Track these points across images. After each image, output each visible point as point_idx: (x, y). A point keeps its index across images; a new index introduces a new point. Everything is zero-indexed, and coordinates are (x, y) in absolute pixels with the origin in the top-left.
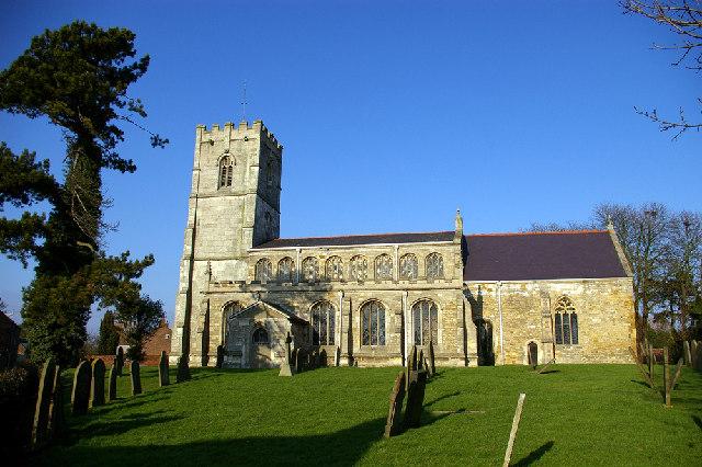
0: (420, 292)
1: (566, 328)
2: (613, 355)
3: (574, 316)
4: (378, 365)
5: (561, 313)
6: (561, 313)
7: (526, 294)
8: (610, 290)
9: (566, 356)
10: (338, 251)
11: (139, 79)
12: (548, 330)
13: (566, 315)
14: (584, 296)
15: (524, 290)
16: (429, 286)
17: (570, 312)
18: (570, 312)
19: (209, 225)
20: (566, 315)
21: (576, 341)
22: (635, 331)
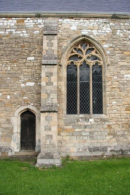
3: (98, 77)
6: (78, 63)
7: (24, 34)
12: (54, 86)
13: (85, 65)
14: (113, 36)
17: (91, 63)
21: (99, 109)
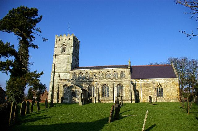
0: (119, 82)
1: (160, 92)
2: (173, 99)
3: (162, 89)
4: (107, 102)
5: (158, 88)
6: (158, 88)
7: (148, 83)
8: (172, 81)
9: (160, 100)
10: (95, 70)
11: (39, 22)
12: (155, 93)
13: (160, 88)
14: (165, 83)
15: (148, 81)
16: (121, 80)
17: (161, 88)
18: (161, 88)
19: (59, 63)
20: (160, 88)
21: (162, 96)
22: (179, 93)
